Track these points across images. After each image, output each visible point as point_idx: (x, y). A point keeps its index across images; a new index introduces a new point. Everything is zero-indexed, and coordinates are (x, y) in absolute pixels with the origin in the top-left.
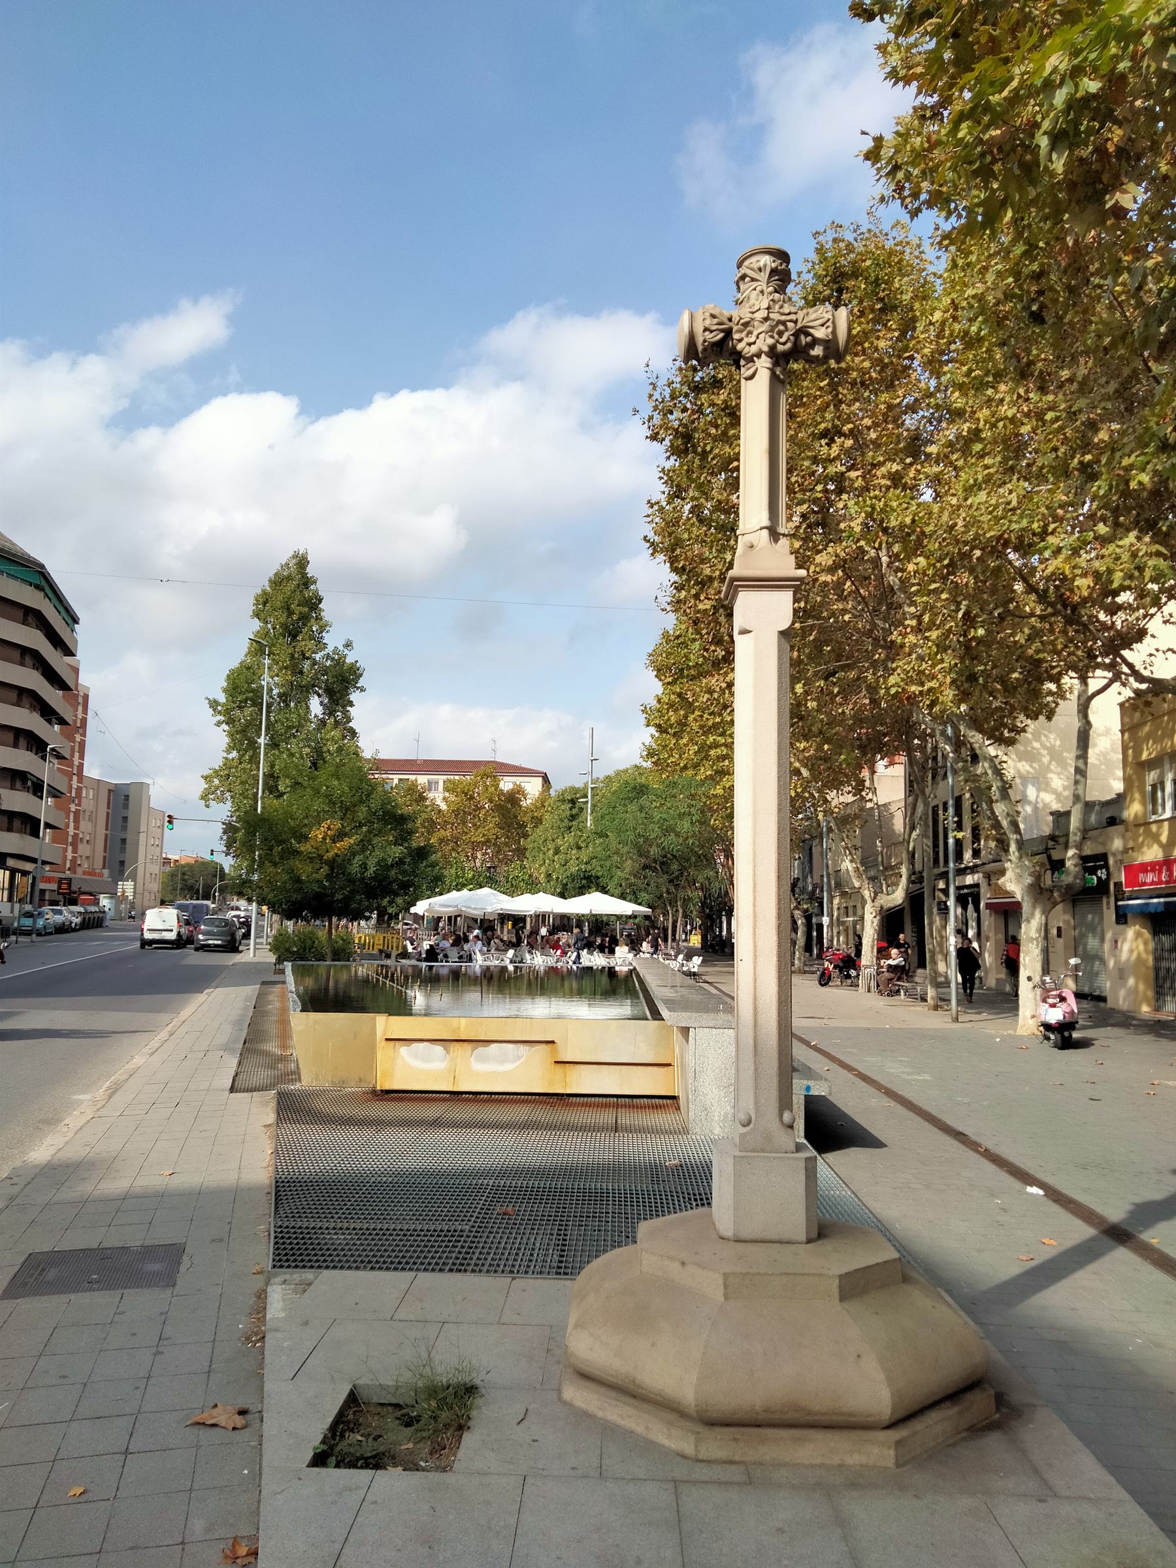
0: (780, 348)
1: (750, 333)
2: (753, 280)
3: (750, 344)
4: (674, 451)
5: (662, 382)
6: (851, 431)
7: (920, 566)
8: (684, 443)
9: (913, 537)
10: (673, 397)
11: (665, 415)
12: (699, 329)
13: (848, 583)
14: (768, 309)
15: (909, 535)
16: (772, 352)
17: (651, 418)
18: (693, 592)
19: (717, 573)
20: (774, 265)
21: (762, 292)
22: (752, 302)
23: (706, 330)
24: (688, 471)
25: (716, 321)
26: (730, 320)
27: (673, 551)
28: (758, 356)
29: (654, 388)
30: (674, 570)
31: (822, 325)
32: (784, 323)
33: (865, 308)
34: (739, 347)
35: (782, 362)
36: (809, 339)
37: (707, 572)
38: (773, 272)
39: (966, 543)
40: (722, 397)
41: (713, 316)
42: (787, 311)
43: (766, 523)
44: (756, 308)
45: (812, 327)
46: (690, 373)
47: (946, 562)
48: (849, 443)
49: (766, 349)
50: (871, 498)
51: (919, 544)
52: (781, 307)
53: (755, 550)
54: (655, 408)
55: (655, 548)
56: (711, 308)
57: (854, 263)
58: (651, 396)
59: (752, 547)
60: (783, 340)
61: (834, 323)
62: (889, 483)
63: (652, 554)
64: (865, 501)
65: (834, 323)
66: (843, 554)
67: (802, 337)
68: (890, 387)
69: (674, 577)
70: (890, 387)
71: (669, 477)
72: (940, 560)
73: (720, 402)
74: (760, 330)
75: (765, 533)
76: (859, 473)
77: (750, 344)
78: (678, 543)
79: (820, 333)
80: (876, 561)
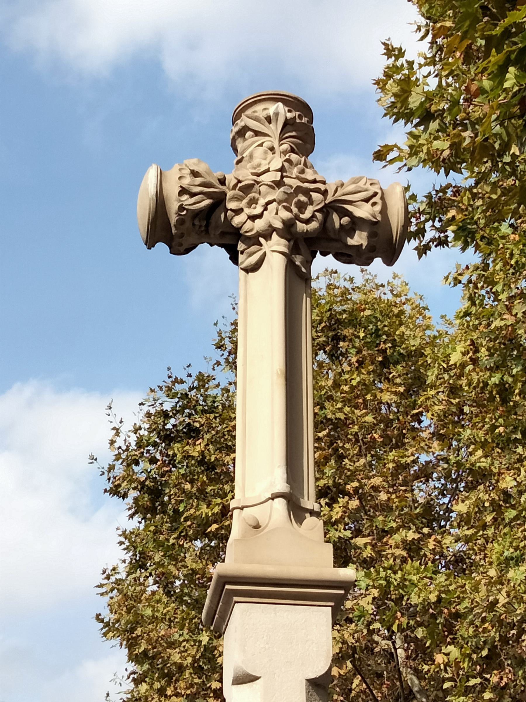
0: (301, 227)
1: (253, 202)
2: (257, 133)
3: (253, 218)
4: (139, 509)
5: (126, 428)
6: (356, 490)
7: (452, 657)
8: (151, 500)
9: (440, 620)
10: (140, 445)
11: (129, 465)
12: (172, 190)
13: (357, 681)
14: (282, 170)
15: (434, 617)
16: (288, 230)
17: (111, 468)
18: (157, 685)
19: (190, 660)
20: (289, 115)
21: (272, 149)
22: (256, 161)
23: (183, 191)
24: (155, 533)
25: (199, 180)
26: (222, 182)
27: (132, 630)
28: (267, 236)
29: (117, 434)
30: (133, 658)
31: (367, 200)
32: (307, 192)
33: (364, 358)
34: (237, 221)
35: (303, 247)
36: (345, 220)
37: (176, 658)
38: (288, 124)
39: (512, 626)
40: (198, 448)
41: (195, 174)
42: (310, 177)
43: (282, 486)
44: (262, 169)
45: (350, 203)
46: (160, 421)
47: (485, 653)
48: (354, 503)
49: (278, 225)
50: (385, 569)
51: (450, 629)
52: (302, 172)
53: (262, 533)
54: (118, 457)
55: (109, 628)
56: (193, 163)
57: (351, 313)
58: (112, 442)
59: (257, 527)
60: (307, 214)
61: (382, 198)
62: (404, 553)
63: (105, 635)
64: (378, 573)
65: (382, 198)
66: (351, 640)
67: (335, 217)
68: (400, 445)
69: (132, 667)
70: (400, 445)
71: (130, 539)
72: (477, 649)
73: (196, 454)
74: (269, 198)
75: (280, 504)
76: (367, 540)
77: (253, 218)
78: (138, 621)
79: (363, 211)
80: (390, 656)
